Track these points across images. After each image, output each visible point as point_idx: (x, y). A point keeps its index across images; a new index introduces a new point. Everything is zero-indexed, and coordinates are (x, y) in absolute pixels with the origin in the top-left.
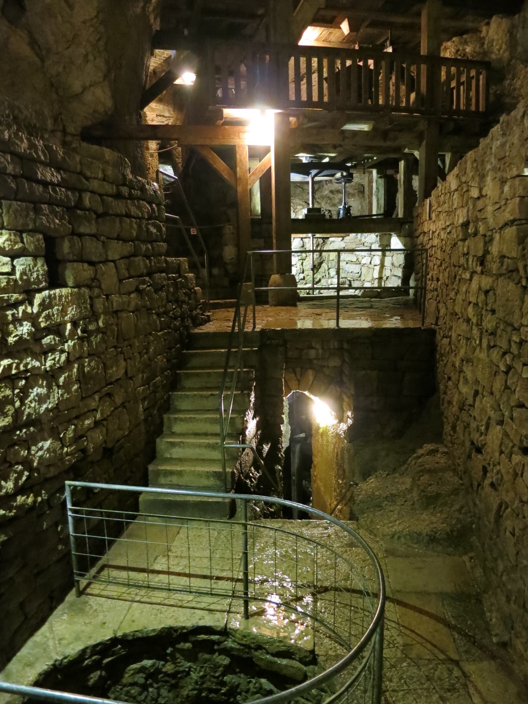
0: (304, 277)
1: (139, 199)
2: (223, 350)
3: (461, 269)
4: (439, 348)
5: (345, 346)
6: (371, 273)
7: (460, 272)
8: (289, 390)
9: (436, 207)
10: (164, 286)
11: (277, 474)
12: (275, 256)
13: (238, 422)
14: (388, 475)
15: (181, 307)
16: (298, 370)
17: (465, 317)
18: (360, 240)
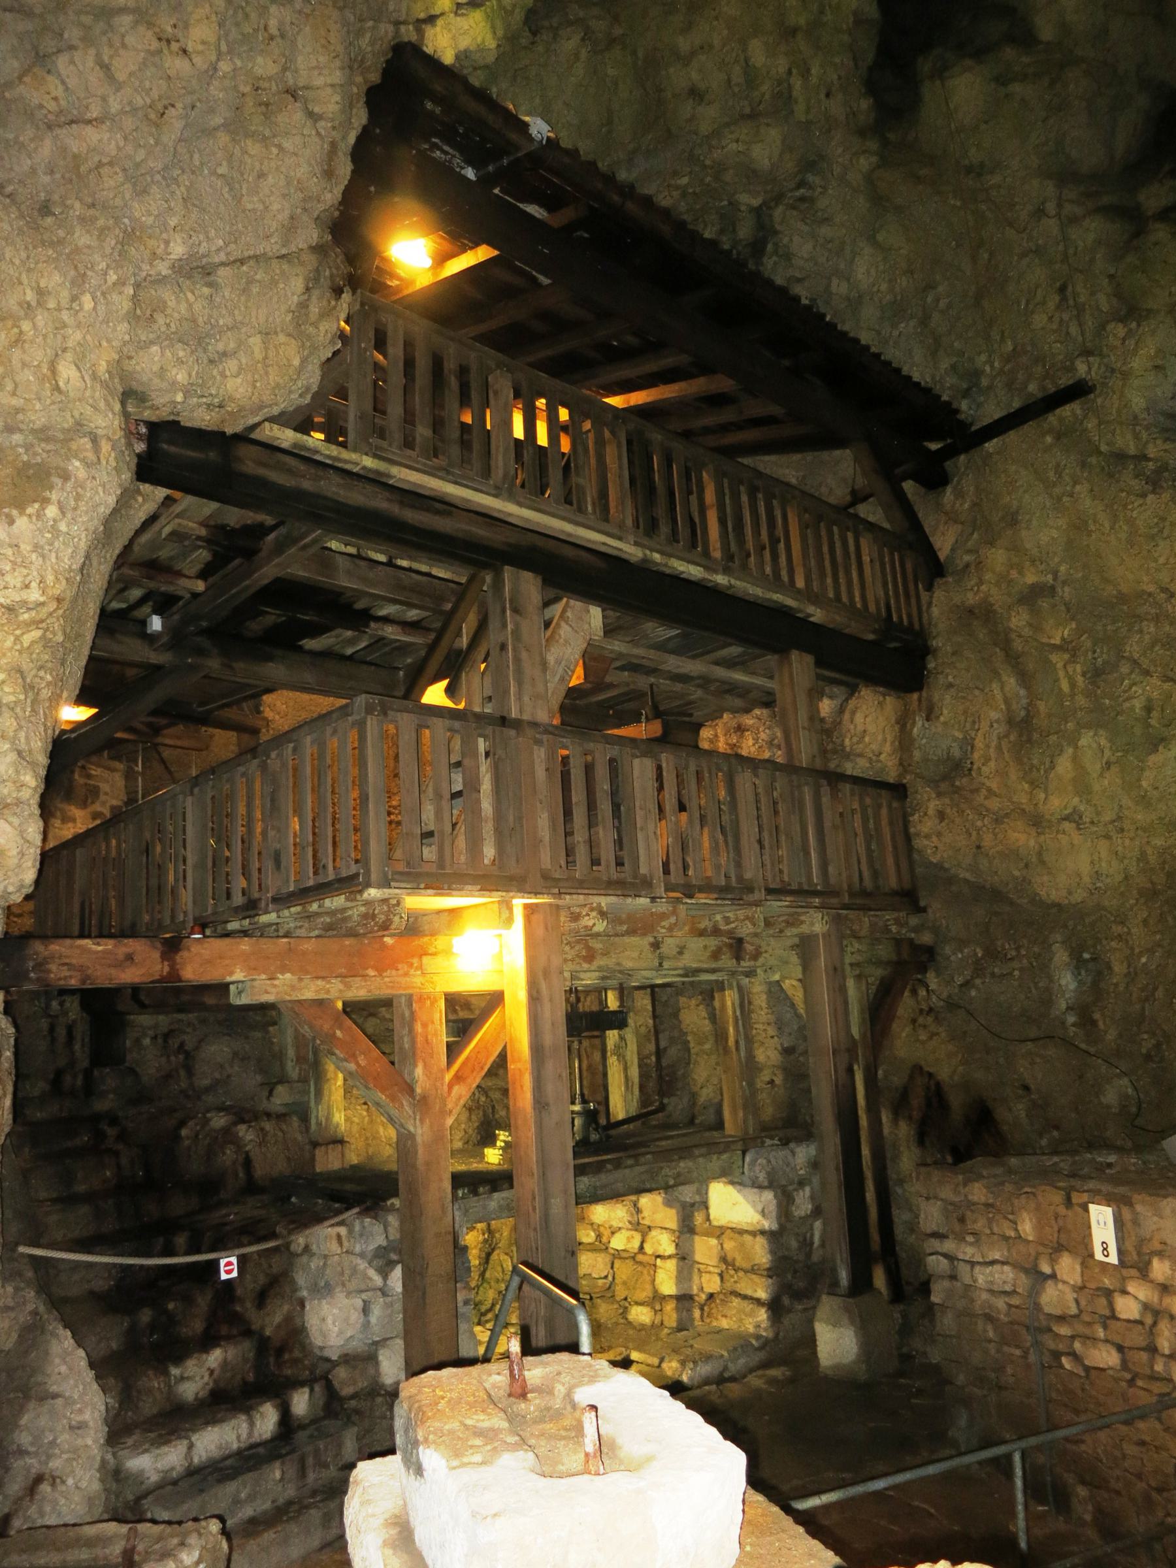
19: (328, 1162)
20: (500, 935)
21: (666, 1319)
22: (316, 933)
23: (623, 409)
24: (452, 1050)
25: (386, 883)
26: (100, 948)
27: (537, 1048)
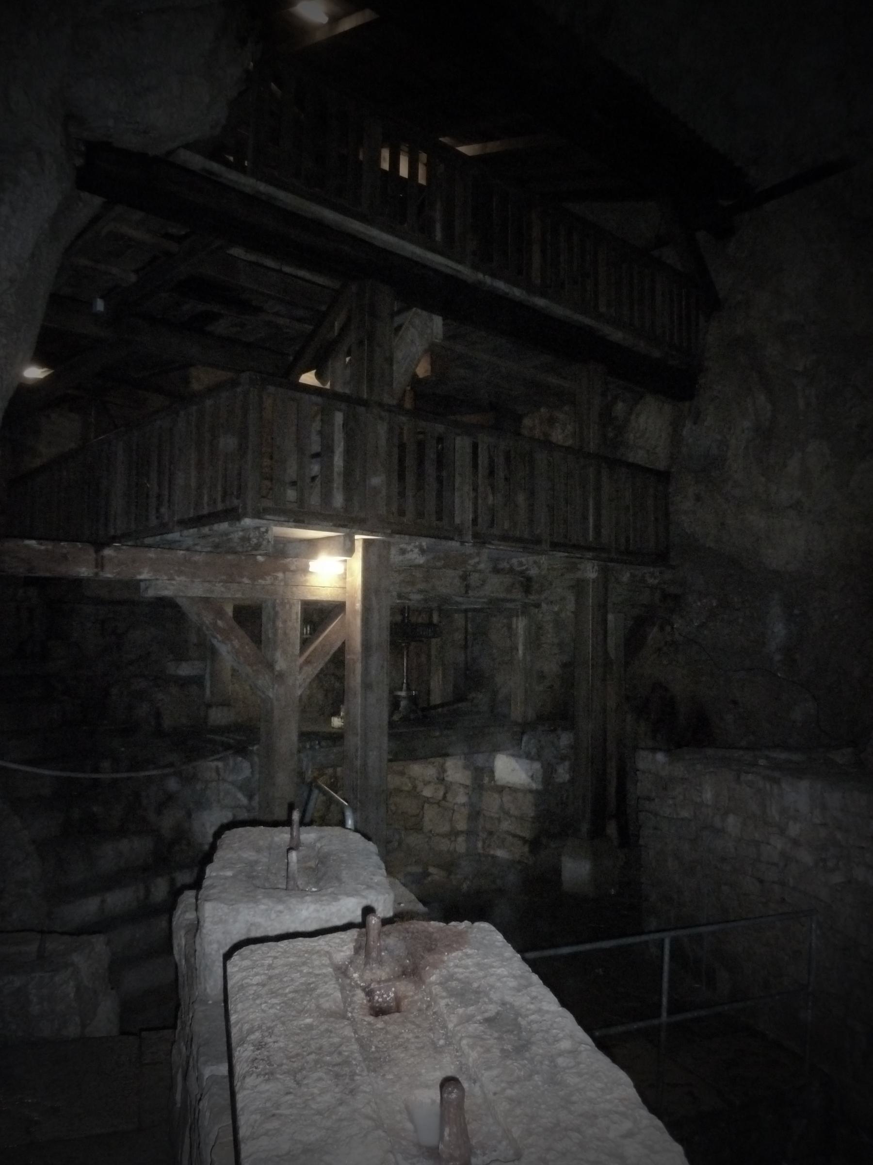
19: (218, 716)
20: (345, 561)
22: (209, 549)
23: (470, 157)
24: (305, 643)
25: (258, 514)
26: (43, 548)
27: (367, 646)
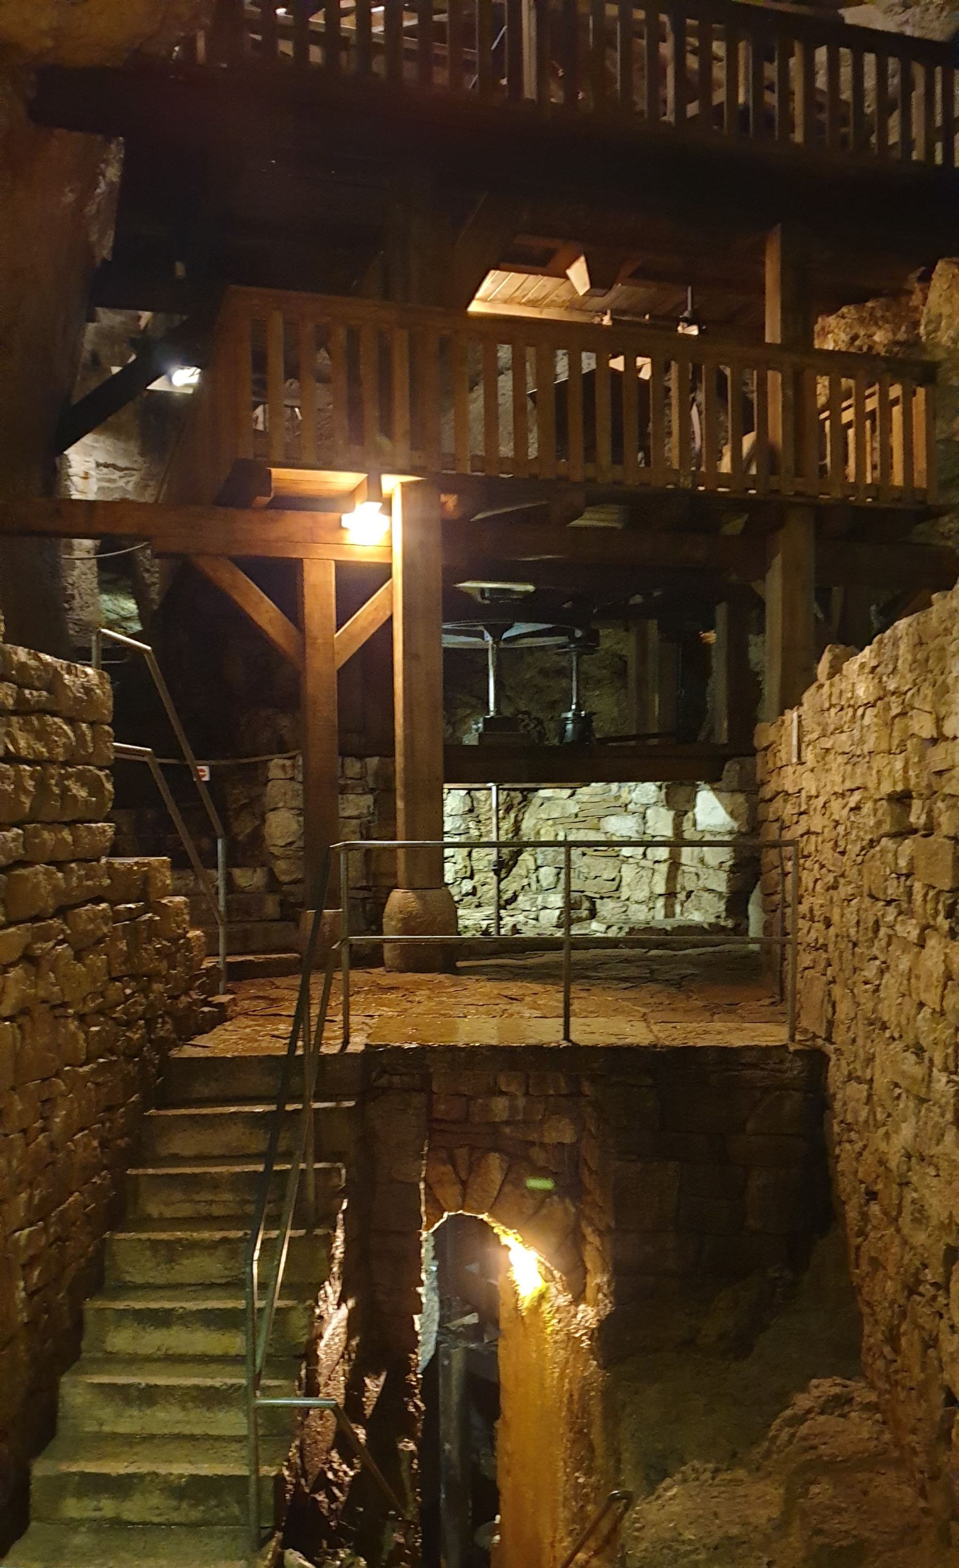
0: (474, 888)
1: (43, 711)
2: (259, 1109)
3: (892, 911)
4: (838, 1105)
5: (587, 1088)
6: (647, 880)
7: (890, 918)
8: (437, 1208)
9: (815, 735)
10: (100, 940)
11: (404, 1466)
12: (401, 853)
13: (298, 1320)
14: (716, 1471)
15: (145, 991)
16: (462, 1154)
17: (910, 1038)
18: (617, 798)
21: (656, 914)
